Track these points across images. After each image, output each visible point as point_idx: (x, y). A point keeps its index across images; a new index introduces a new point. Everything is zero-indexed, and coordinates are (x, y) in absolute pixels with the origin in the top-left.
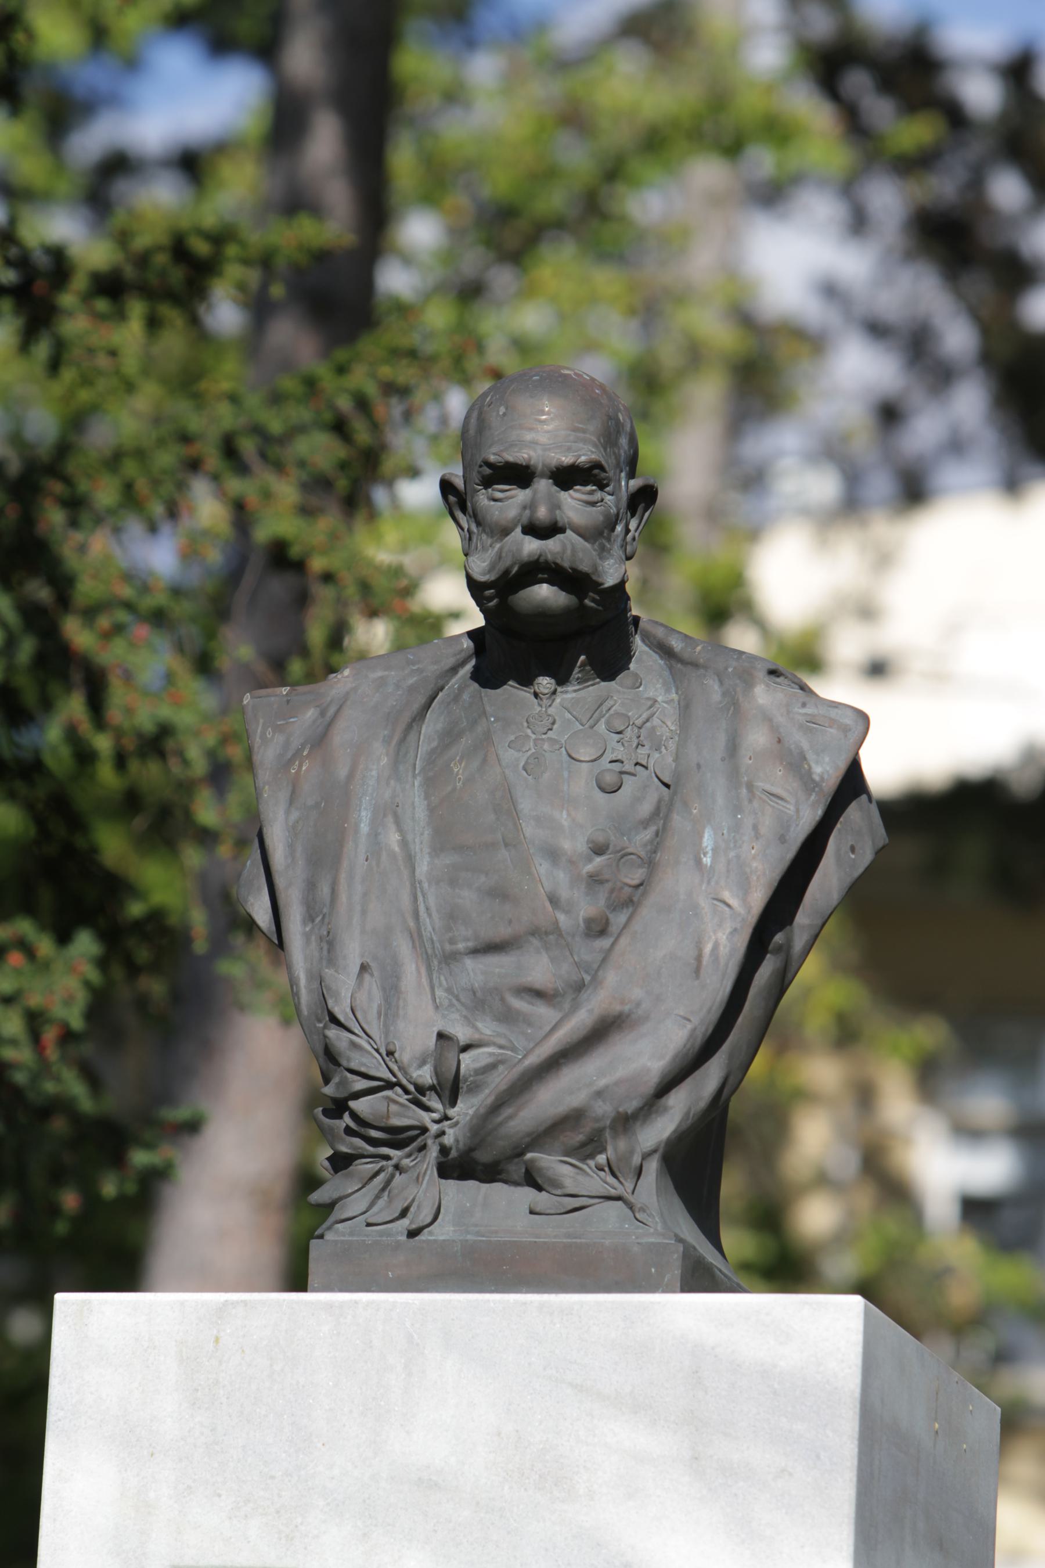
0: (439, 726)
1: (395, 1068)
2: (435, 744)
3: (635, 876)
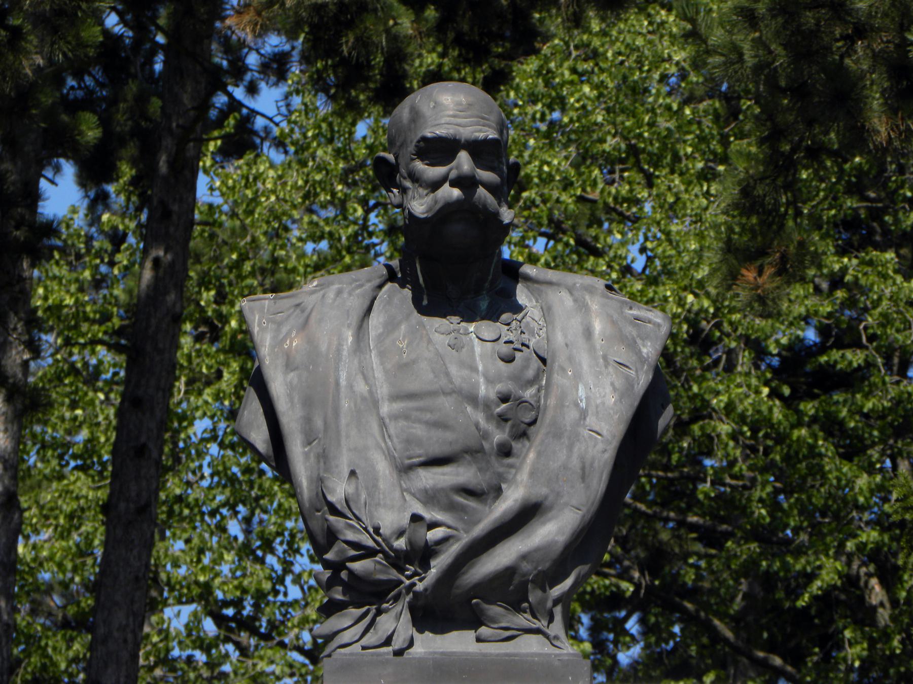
0: (381, 320)
1: (379, 539)
2: (381, 330)
3: (528, 418)
